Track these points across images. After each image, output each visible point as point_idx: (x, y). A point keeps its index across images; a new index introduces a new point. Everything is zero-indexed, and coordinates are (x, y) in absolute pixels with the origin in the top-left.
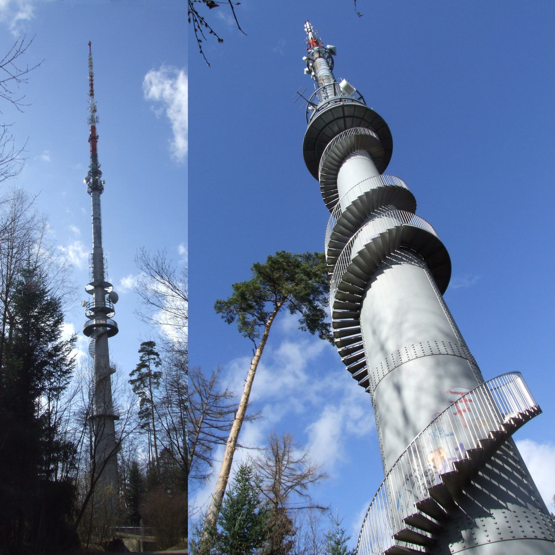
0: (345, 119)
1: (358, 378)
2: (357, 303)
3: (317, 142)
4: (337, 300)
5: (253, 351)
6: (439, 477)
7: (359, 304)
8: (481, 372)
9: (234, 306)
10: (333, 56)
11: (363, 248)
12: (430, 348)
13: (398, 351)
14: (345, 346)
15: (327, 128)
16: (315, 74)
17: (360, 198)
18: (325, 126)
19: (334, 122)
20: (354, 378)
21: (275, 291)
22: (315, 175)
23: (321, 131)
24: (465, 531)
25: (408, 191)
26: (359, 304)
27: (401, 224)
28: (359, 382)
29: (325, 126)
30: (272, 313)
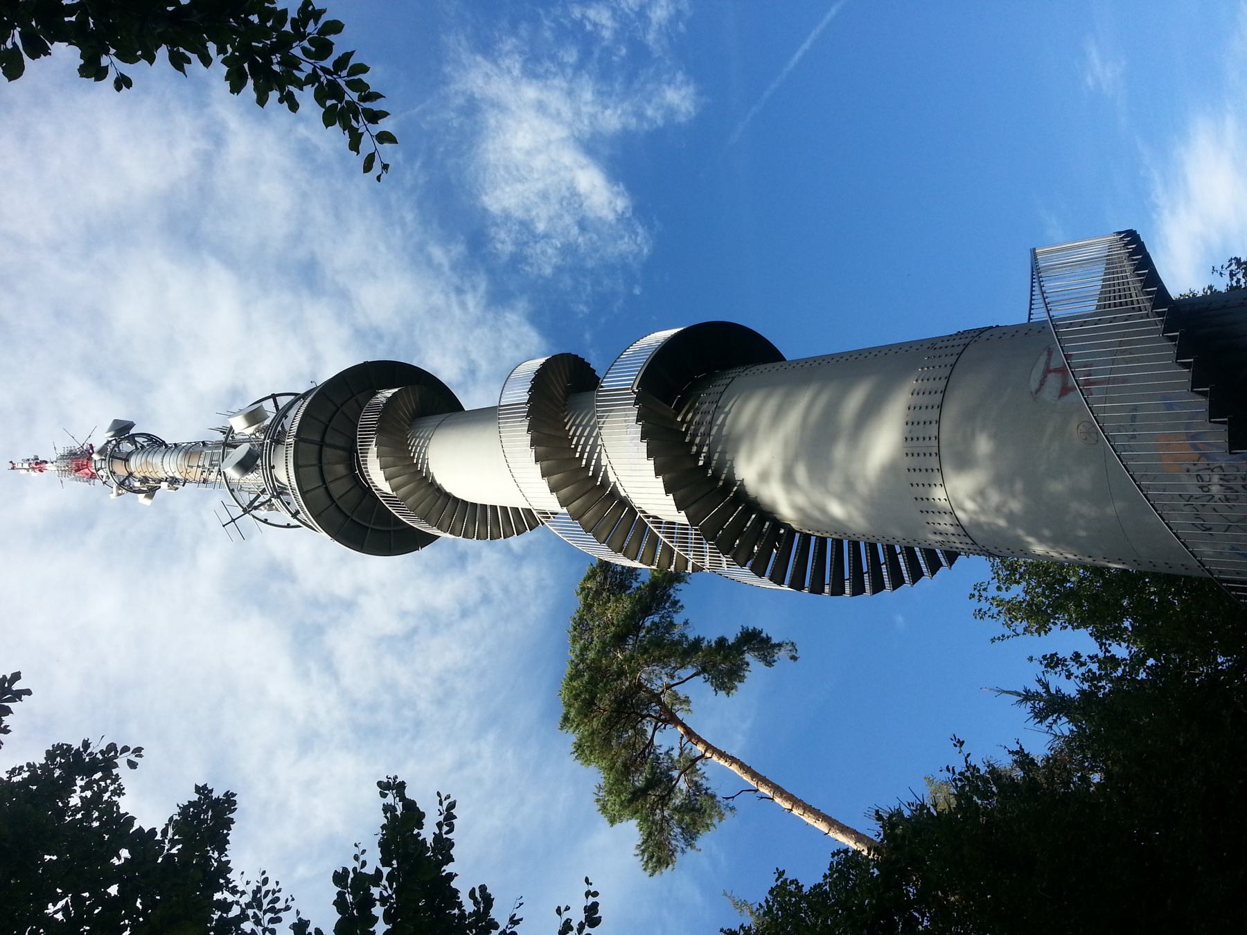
0: (318, 444)
1: (934, 566)
2: (766, 527)
3: (354, 518)
4: (749, 563)
5: (762, 798)
6: (1235, 456)
7: (767, 523)
8: (997, 326)
9: (1217, 497)
10: (132, 431)
11: (661, 479)
12: (924, 408)
13: (909, 470)
14: (843, 580)
15: (331, 487)
16: (166, 481)
17: (538, 459)
18: (327, 489)
19: (325, 467)
20: (933, 572)
21: (610, 724)
22: (430, 539)
23: (333, 501)
24: (727, 455)
25: (553, 357)
26: (767, 523)
27: (633, 392)
28: (944, 563)
29: (327, 489)
30: (682, 738)
